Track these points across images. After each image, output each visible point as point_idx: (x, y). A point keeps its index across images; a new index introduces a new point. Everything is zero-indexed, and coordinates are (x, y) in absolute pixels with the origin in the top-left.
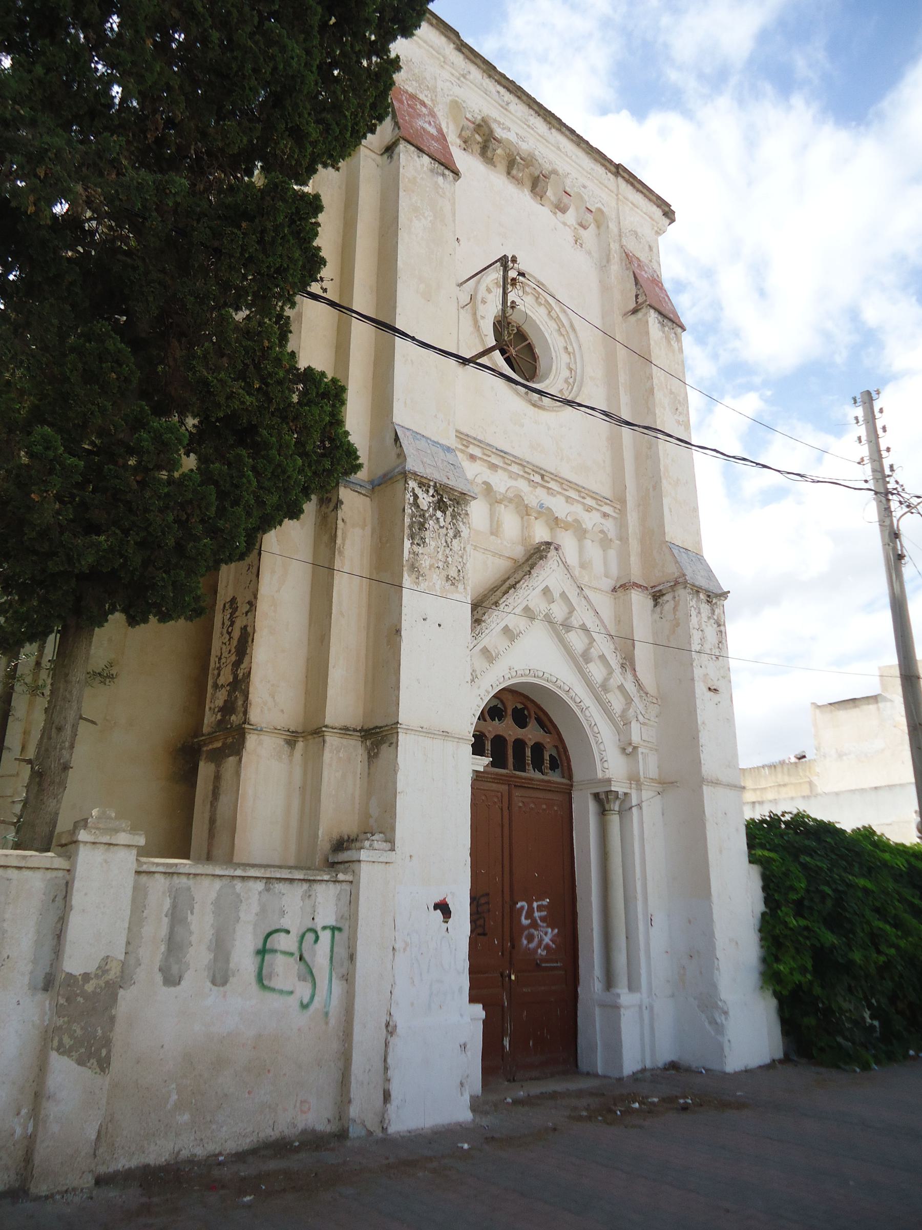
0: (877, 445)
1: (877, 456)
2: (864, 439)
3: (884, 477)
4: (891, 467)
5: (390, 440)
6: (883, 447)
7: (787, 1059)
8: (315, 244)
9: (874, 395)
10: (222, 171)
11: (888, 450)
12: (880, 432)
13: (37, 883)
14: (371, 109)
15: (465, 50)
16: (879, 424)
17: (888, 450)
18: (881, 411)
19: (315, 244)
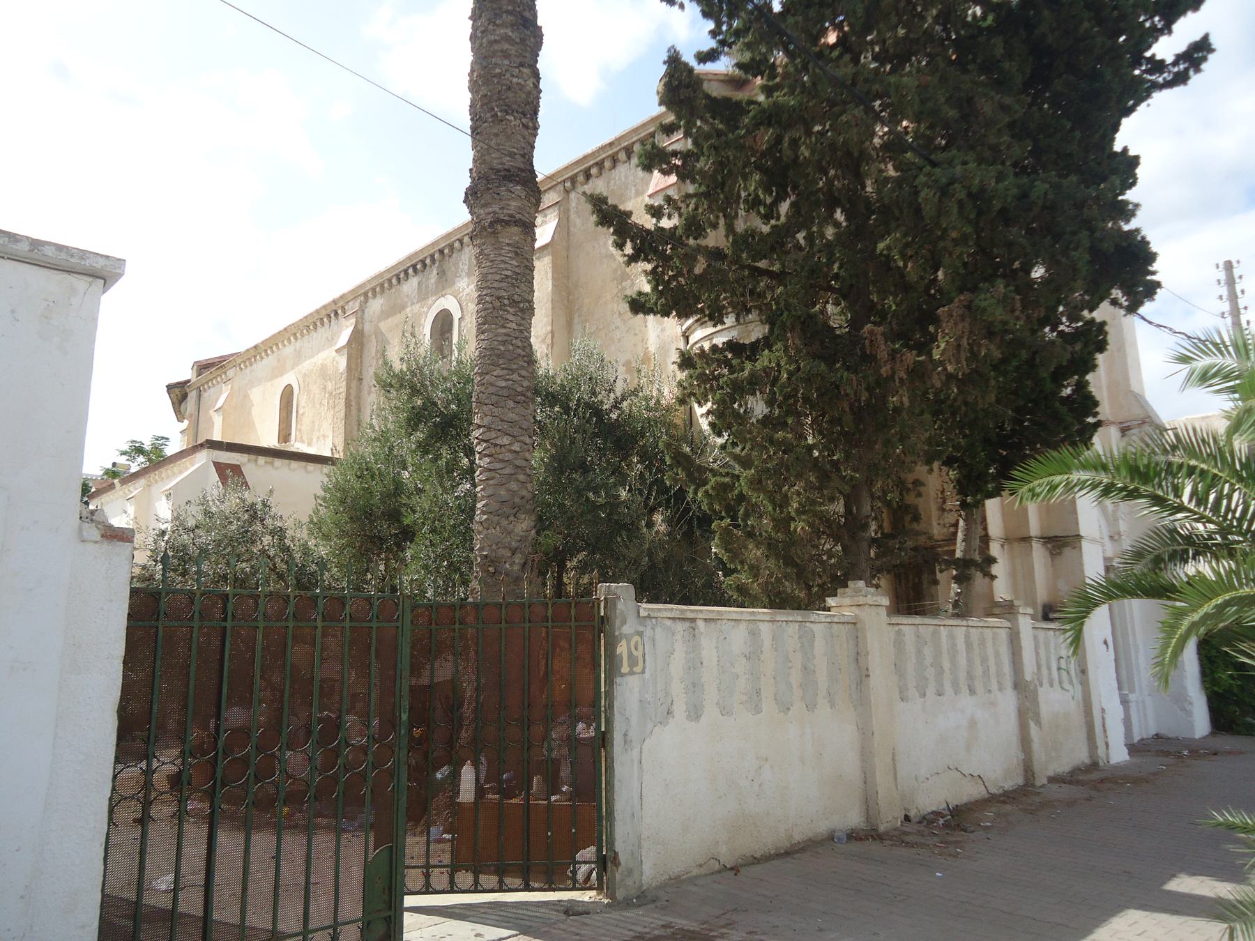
0: (1237, 304)
1: (1236, 312)
2: (1225, 297)
3: (1241, 330)
4: (1248, 322)
5: (855, 847)
6: (1241, 305)
7: (1212, 734)
8: (1117, 147)
9: (1235, 264)
10: (825, 447)
11: (1240, 277)
12: (1239, 294)
13: (1003, 634)
14: (412, 673)
15: (354, 384)
16: (1238, 288)
17: (1240, 277)
18: (1243, 292)
19: (1117, 147)
